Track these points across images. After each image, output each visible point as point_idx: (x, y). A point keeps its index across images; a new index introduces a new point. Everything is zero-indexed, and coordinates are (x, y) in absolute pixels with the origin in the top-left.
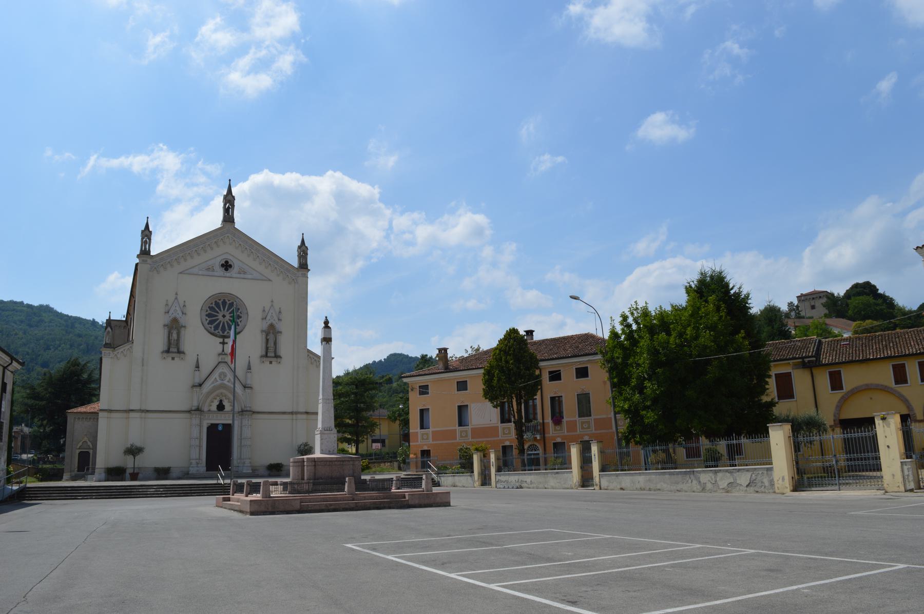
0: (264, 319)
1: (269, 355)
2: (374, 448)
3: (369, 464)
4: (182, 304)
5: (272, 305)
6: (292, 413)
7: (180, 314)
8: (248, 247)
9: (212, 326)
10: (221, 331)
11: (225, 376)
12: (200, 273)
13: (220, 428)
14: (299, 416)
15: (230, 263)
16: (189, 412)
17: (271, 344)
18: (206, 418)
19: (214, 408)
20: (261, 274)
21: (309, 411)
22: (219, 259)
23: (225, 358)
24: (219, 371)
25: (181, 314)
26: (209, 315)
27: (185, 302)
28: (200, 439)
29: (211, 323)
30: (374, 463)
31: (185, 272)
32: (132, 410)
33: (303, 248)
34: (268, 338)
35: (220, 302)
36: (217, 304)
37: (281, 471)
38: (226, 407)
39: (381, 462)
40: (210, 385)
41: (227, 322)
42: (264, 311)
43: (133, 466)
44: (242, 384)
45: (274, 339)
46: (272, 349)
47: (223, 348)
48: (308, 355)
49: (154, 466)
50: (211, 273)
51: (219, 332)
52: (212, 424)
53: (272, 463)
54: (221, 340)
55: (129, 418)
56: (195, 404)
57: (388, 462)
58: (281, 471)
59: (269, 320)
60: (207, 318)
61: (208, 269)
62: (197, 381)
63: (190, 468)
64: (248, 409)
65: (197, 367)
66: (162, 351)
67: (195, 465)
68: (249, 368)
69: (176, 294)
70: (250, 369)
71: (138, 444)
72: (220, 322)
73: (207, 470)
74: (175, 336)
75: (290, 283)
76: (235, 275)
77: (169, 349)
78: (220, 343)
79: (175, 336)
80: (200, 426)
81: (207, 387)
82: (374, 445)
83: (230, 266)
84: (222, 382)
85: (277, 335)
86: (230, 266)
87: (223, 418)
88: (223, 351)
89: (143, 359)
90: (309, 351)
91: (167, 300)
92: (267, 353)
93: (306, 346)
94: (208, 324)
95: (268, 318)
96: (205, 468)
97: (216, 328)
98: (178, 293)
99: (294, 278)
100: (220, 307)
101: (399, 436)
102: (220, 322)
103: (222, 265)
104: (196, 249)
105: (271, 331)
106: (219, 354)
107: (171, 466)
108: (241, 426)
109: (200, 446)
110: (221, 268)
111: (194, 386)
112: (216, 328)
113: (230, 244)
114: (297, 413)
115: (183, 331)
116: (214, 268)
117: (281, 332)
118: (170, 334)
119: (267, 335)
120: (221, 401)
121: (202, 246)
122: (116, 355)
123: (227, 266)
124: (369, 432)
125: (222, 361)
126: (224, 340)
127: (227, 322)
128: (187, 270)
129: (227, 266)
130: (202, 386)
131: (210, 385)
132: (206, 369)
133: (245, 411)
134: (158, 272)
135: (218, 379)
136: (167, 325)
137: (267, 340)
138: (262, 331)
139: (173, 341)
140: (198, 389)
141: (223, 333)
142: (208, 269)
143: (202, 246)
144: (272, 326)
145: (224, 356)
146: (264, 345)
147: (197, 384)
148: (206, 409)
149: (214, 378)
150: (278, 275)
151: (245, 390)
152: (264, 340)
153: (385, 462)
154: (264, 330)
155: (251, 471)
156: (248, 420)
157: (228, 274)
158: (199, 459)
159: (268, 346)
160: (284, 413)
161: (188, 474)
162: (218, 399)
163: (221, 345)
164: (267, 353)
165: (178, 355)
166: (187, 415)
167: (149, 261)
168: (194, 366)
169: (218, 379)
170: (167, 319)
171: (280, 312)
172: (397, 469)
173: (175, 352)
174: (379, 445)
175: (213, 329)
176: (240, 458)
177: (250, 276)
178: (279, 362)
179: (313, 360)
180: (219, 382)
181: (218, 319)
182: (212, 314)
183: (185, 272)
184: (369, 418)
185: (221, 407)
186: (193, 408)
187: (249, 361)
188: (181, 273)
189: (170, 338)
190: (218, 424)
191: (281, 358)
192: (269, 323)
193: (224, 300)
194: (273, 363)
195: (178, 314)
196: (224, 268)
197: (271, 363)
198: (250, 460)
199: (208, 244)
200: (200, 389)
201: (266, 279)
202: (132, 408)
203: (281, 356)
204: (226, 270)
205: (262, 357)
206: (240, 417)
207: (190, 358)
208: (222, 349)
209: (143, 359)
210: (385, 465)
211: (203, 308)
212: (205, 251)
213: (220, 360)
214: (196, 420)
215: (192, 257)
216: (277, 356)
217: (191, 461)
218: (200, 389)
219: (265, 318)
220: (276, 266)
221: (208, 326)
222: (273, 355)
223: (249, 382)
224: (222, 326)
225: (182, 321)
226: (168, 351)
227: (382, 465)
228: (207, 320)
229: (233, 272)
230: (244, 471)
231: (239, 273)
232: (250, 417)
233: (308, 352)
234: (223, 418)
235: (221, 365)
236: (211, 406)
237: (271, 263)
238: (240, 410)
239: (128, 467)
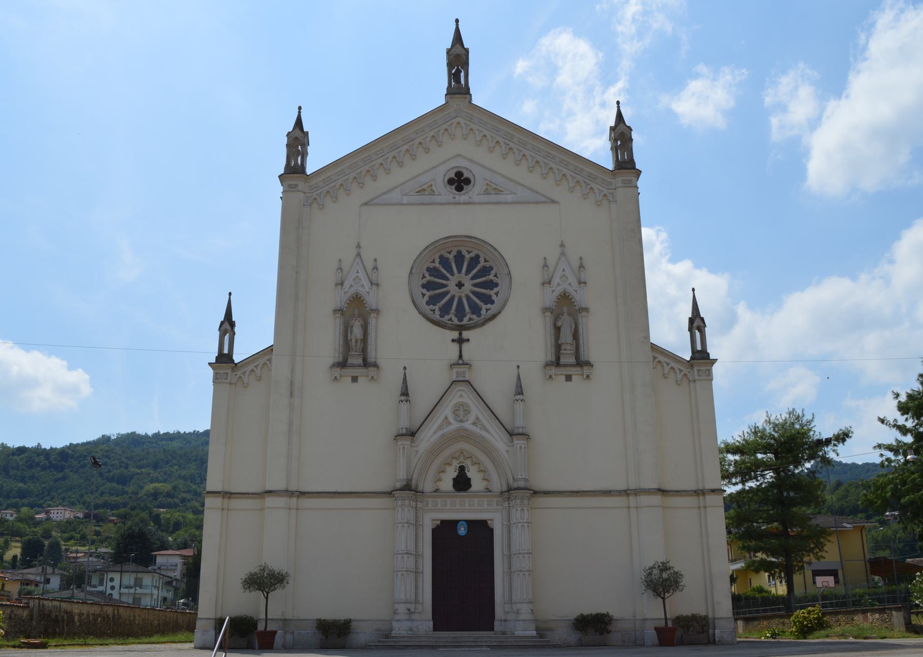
0: (547, 282)
2: (819, 584)
3: (824, 614)
4: (369, 265)
5: (563, 254)
6: (626, 493)
7: (365, 285)
8: (501, 140)
9: (437, 308)
10: (456, 316)
11: (467, 411)
12: (405, 200)
13: (462, 530)
14: (644, 500)
15: (465, 176)
16: (390, 494)
17: (566, 337)
19: (447, 484)
20: (531, 190)
21: (667, 487)
22: (442, 170)
23: (464, 373)
24: (455, 401)
26: (428, 286)
27: (375, 260)
28: (417, 556)
29: (432, 301)
30: (836, 613)
31: (376, 201)
32: (270, 492)
33: (621, 127)
34: (559, 324)
35: (451, 257)
36: (444, 261)
37: (609, 632)
38: (473, 483)
39: (855, 612)
40: (435, 433)
41: (453, 275)
42: (545, 266)
43: (663, 617)
44: (507, 431)
45: (573, 327)
46: (569, 347)
47: (461, 351)
48: (655, 358)
49: (316, 618)
50: (426, 198)
51: (450, 319)
52: (442, 522)
53: (585, 613)
54: (455, 335)
55: (264, 509)
56: (402, 475)
57: (873, 611)
58: (609, 632)
59: (559, 284)
60: (424, 291)
61: (421, 192)
62: (404, 424)
63: (394, 623)
64: (521, 484)
65: (405, 393)
66: (331, 364)
68: (519, 391)
69: (359, 246)
70: (521, 393)
71: (276, 564)
72: (453, 298)
73: (436, 628)
74: (357, 332)
75: (598, 204)
76: (477, 199)
78: (453, 341)
79: (357, 332)
80: (417, 525)
81: (427, 438)
82: (820, 580)
83: (468, 181)
85: (580, 316)
86: (468, 181)
88: (461, 357)
89: (292, 383)
90: (655, 348)
91: (340, 260)
92: (558, 358)
93: (647, 337)
94: (428, 303)
95: (556, 280)
97: (445, 310)
98: (361, 245)
99: (606, 191)
100: (451, 267)
101: (863, 562)
102: (453, 298)
103: (451, 182)
104: (393, 154)
105: (565, 309)
106: (452, 366)
107: (352, 618)
108: (509, 525)
109: (417, 573)
110: (448, 187)
111: (399, 436)
112: (445, 310)
113: (465, 137)
114: (637, 492)
115: (372, 321)
116: (434, 188)
117: (586, 310)
118: (347, 329)
119: (556, 319)
120: (462, 469)
121: (406, 147)
122: (240, 377)
123: (459, 182)
124: (813, 549)
125: (458, 379)
126: (460, 334)
127: (453, 275)
128: (379, 196)
129: (459, 182)
131: (435, 433)
132: (423, 397)
134: (322, 207)
137: (557, 330)
138: (545, 310)
140: (406, 442)
141: (461, 320)
142: (421, 192)
143: (406, 147)
144: (565, 298)
145: (461, 369)
146: (550, 340)
147: (404, 431)
148: (428, 487)
149: (442, 418)
150: (572, 190)
151: (512, 441)
153: (864, 612)
154: (548, 306)
155: (534, 633)
157: (462, 197)
160: (607, 493)
161: (387, 636)
162: (456, 464)
163: (456, 346)
164: (558, 358)
165: (365, 370)
166: (386, 502)
167: (301, 185)
168: (399, 393)
170: (338, 298)
171: (581, 266)
172: (903, 629)
173: (359, 366)
174: (831, 579)
175: (437, 312)
176: (511, 602)
177: (509, 198)
178: (588, 376)
179: (667, 369)
180: (455, 425)
181: (447, 293)
183: (376, 201)
184: (810, 519)
185: (462, 483)
186: (398, 485)
187: (519, 376)
188: (366, 204)
189: (349, 338)
191: (592, 366)
192: (559, 291)
193: (459, 252)
194: (574, 377)
195: (363, 286)
196: (454, 187)
197: (569, 378)
198: (531, 606)
199: (417, 142)
200: (412, 442)
201: (543, 199)
202: (269, 487)
203: (591, 360)
204: (459, 189)
205: (547, 365)
206: (506, 504)
207: (391, 377)
208: (458, 354)
209: (292, 383)
210: (866, 619)
211: (414, 271)
212: (414, 157)
213: (454, 378)
215: (388, 171)
216: (582, 363)
218: (412, 442)
219: (549, 283)
220: (565, 171)
221: (427, 309)
222: (572, 360)
223: (519, 422)
224: (457, 306)
225: (371, 301)
226: (342, 364)
227: (858, 618)
228: (424, 295)
229: (473, 192)
230: (517, 633)
231: (486, 193)
232: (526, 502)
233: (652, 347)
236: (440, 480)
237: (552, 165)
238: (505, 488)
239: (260, 618)
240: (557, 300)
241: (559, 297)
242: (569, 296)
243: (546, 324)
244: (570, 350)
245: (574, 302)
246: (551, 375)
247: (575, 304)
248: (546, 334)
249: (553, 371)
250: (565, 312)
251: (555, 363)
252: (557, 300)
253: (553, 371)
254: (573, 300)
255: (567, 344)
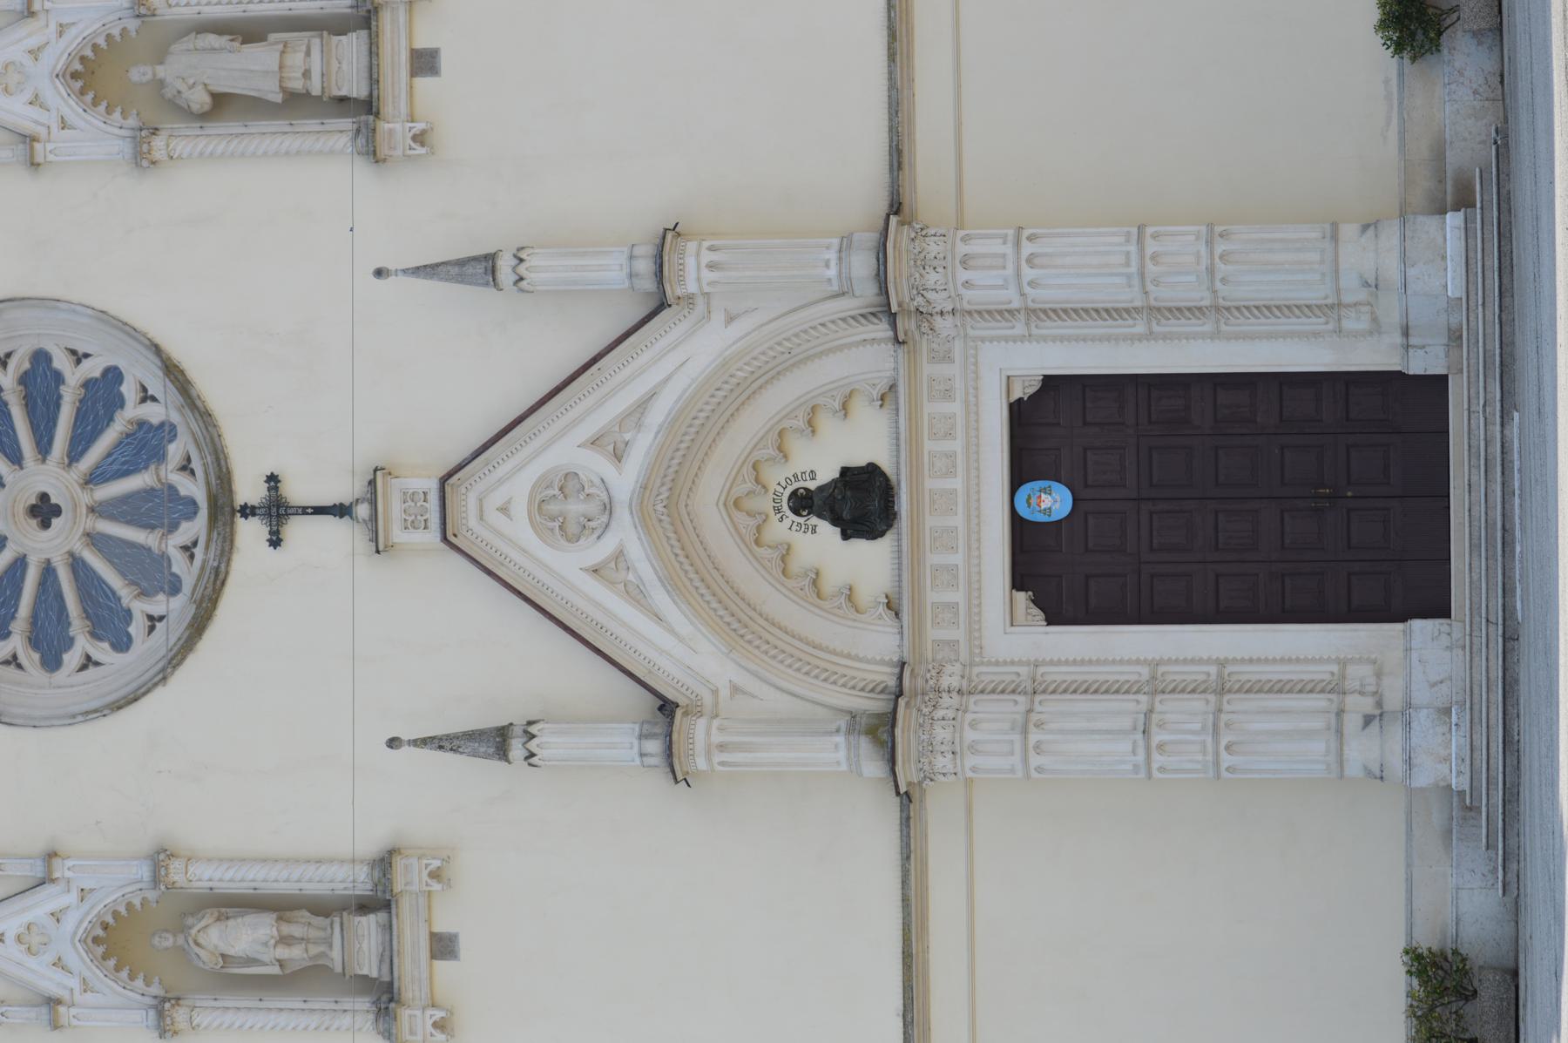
1: (355, 88)
9: (140, 608)
10: (173, 527)
11: (568, 484)
18: (958, 634)
23: (412, 496)
25: (48, 889)
28: (1157, 685)
34: (199, 100)
38: (859, 460)
46: (296, 60)
47: (319, 511)
51: (188, 549)
54: (250, 532)
59: (35, 101)
60: (72, 659)
63: (1422, 779)
64: (862, 265)
65: (497, 741)
66: (363, 171)
67: (1396, 732)
70: (488, 263)
77: (365, 984)
84: (623, 517)
87: (957, 483)
88: (340, 511)
94: (122, 643)
96: (1421, 628)
105: (140, 74)
106: (378, 545)
107: (1401, 944)
120: (803, 502)
126: (247, 511)
130: (670, 694)
133: (883, 289)
135: (600, 551)
136: (161, 1014)
137: (221, 104)
139: (283, 952)
140: (697, 734)
145: (393, 508)
146: (268, 136)
152: (221, 136)
154: (127, 148)
156: (965, 262)
158: (1336, 688)
159: (278, 98)
162: (784, 527)
163: (297, 530)
165: (405, 908)
168: (497, 765)
169: (600, 551)
175: (158, 605)
180: (625, 534)
182: (34, 619)
186: (873, 767)
187: (417, 271)
189: (276, 970)
190: (1018, 523)
192: (61, 101)
195: (57, 917)
198: (1349, 231)
200: (695, 711)
203: (371, 843)
213: (433, 535)
214: (973, 748)
217: (1353, 769)
218: (695, 711)
221: (147, 648)
222: (352, 46)
228: (88, 662)
232: (933, 248)
234: (957, 483)
235: (473, 522)
236: (850, 594)
238: (881, 329)
240: (102, 108)
241: (89, 97)
242: (83, 59)
243: (201, 154)
244: (308, 53)
245: (109, 37)
246: (415, 138)
247: (116, 32)
248: (243, 155)
249: (397, 126)
250: (149, 76)
251: (363, 118)
252: (102, 108)
253: (397, 126)
254: (101, 41)
255: (281, 67)
